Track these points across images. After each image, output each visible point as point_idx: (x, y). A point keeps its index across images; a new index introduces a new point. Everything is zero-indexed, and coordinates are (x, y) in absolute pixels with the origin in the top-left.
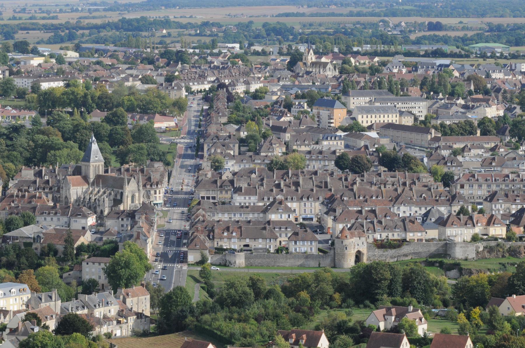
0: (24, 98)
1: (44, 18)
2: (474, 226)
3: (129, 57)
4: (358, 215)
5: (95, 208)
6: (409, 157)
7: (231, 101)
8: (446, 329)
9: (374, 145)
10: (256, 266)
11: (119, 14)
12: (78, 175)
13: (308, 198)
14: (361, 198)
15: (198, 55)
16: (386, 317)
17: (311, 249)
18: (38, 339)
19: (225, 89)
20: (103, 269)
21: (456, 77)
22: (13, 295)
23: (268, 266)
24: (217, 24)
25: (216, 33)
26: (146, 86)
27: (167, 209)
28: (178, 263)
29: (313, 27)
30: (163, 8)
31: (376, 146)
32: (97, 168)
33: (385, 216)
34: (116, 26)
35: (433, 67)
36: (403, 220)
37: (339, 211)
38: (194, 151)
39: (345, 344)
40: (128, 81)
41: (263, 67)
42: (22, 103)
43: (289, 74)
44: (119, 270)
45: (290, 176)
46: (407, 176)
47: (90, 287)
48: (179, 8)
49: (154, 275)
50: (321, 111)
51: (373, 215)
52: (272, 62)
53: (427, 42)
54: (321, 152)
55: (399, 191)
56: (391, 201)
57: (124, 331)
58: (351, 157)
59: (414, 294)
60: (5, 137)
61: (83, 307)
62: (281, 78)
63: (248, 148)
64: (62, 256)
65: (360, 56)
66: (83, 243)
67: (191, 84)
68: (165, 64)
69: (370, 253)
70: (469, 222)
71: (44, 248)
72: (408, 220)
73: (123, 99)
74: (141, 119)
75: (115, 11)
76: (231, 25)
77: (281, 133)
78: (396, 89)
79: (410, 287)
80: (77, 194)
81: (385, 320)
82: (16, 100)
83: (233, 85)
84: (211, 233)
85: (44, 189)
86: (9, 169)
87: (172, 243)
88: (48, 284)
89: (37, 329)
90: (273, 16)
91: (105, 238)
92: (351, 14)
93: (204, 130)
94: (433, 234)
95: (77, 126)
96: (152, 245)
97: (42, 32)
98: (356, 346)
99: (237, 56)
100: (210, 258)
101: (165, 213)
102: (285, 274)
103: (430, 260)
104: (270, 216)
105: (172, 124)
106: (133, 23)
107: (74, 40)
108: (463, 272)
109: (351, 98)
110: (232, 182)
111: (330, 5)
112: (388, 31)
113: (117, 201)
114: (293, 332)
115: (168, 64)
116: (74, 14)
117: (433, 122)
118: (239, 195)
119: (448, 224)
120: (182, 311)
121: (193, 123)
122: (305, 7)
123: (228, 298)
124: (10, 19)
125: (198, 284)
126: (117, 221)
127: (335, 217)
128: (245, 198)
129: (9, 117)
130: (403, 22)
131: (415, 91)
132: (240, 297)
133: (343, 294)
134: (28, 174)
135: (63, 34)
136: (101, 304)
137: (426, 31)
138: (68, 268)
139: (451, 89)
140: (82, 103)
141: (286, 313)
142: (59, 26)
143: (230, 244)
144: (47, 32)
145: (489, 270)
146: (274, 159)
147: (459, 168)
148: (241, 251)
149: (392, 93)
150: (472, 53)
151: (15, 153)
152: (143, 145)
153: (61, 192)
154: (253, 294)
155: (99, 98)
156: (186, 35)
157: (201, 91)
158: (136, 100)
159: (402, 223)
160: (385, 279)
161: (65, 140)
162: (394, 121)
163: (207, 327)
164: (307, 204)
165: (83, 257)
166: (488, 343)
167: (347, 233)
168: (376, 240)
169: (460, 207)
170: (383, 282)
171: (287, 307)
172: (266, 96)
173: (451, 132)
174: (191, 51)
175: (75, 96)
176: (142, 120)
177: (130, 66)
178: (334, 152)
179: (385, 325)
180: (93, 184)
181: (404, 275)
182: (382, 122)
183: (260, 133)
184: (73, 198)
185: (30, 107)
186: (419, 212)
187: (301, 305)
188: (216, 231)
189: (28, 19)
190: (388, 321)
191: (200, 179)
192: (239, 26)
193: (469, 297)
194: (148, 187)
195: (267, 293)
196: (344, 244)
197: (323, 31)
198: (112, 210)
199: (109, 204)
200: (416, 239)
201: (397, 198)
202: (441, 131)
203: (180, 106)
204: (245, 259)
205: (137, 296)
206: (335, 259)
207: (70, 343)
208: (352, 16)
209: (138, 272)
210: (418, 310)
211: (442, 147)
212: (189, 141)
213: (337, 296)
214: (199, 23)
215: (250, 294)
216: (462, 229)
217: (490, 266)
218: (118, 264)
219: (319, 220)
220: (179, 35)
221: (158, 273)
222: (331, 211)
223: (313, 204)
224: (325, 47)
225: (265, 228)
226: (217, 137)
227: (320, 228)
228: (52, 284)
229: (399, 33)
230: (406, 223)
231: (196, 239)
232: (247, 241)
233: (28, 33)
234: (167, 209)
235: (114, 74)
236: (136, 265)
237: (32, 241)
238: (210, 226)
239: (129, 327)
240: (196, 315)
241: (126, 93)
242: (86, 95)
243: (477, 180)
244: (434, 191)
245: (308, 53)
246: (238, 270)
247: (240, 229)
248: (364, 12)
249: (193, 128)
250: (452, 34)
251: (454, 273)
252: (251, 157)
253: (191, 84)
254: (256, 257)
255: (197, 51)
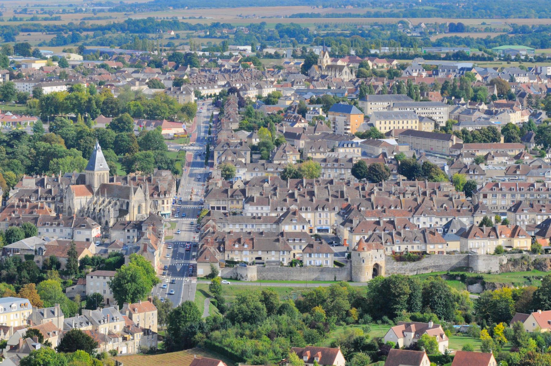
0: (25, 103)
1: (46, 19)
2: (498, 237)
3: (135, 60)
4: (375, 226)
5: (100, 219)
6: (429, 165)
7: (243, 107)
8: (468, 346)
9: (393, 153)
10: (269, 279)
11: (125, 14)
12: (81, 184)
13: (323, 209)
14: (379, 208)
15: (207, 57)
16: (405, 333)
17: (327, 262)
18: (40, 357)
19: (236, 94)
20: (108, 283)
21: (479, 81)
22: (14, 310)
23: (281, 280)
24: (227, 25)
25: (226, 35)
26: (154, 91)
27: (175, 220)
28: (187, 276)
29: (329, 29)
30: (171, 8)
31: (395, 154)
32: (101, 177)
33: (404, 228)
34: (121, 28)
35: (455, 71)
36: (423, 232)
37: (356, 222)
38: (203, 159)
39: (362, 362)
40: (134, 85)
41: (276, 70)
42: (23, 108)
43: (303, 77)
44: (125, 284)
45: (304, 185)
46: (427, 185)
47: (94, 302)
48: (188, 9)
49: (162, 289)
50: (337, 117)
51: (391, 226)
52: (286, 66)
53: (448, 44)
54: (337, 160)
55: (419, 200)
56: (411, 211)
57: (130, 348)
58: (368, 165)
59: (434, 309)
60: (5, 144)
61: (88, 323)
62: (295, 82)
63: (260, 156)
64: (65, 269)
65: (377, 59)
66: (87, 256)
67: (201, 88)
68: (173, 67)
69: (388, 266)
70: (493, 233)
71: (46, 260)
72: (428, 232)
73: (129, 105)
74: (148, 125)
75: (120, 11)
76: (243, 26)
77: (295, 140)
78: (416, 94)
79: (431, 302)
80: (81, 204)
81: (404, 336)
82: (16, 105)
83: (244, 89)
84: (221, 245)
85: (46, 199)
86: (9, 178)
87: (181, 256)
88: (50, 298)
89: (38, 346)
90: (286, 17)
91: (110, 251)
92: (368, 15)
93: (214, 137)
94: (454, 246)
95: (81, 132)
96: (160, 258)
97: (44, 33)
98: (373, 364)
99: (248, 59)
100: (220, 272)
101: (173, 224)
102: (299, 289)
103: (451, 273)
104: (283, 227)
105: (181, 130)
106: (140, 24)
107: (78, 42)
108: (486, 286)
109: (369, 103)
110: (243, 191)
111: (346, 5)
112: (408, 33)
113: (123, 212)
114: (307, 349)
115: (176, 68)
116: (78, 14)
117: (455, 129)
118: (251, 205)
119: (470, 236)
120: (191, 327)
121: (203, 129)
122: (321, 7)
123: (240, 313)
124: (10, 20)
125: (208, 299)
126: (123, 232)
127: (351, 228)
128: (257, 209)
129: (9, 123)
130: (423, 23)
131: (435, 96)
132: (252, 312)
133: (360, 309)
134: (30, 183)
135: (66, 36)
136: (106, 320)
137: (448, 33)
138: (72, 282)
139: (473, 93)
140: (85, 108)
141: (300, 329)
142: (62, 28)
143: (241, 256)
144: (49, 34)
145: (513, 283)
146: (288, 167)
147: (482, 177)
148: (253, 263)
149: (412, 97)
150: (495, 56)
151: (15, 161)
152: (150, 152)
153: (64, 202)
154: (265, 309)
155: (104, 103)
156: (195, 37)
157: (211, 96)
158: (142, 105)
159: (422, 235)
160: (404, 294)
161: (69, 147)
162: (414, 128)
163: (217, 344)
164: (322, 214)
165: (87, 271)
166: (512, 361)
167: (364, 245)
168: (394, 253)
169: (482, 218)
170: (402, 296)
171: (302, 323)
172: (279, 101)
173: (474, 139)
174: (201, 53)
175: (79, 101)
176: (149, 126)
177: (136, 69)
178: (351, 160)
179: (404, 342)
180: (98, 193)
181: (424, 289)
182: (401, 128)
183: (273, 140)
184: (77, 208)
185: (32, 113)
186: (440, 223)
187: (315, 321)
188: (227, 243)
189: (29, 20)
190: (407, 338)
191: (210, 188)
192: (251, 27)
193: (492, 313)
194: (156, 196)
195: (280, 308)
196: (361, 256)
197: (339, 32)
198: (117, 221)
199: (114, 214)
200: (437, 251)
201: (417, 208)
202: (463, 137)
203: (189, 112)
204: (257, 272)
205: (144, 311)
206: (351, 273)
207: (74, 361)
208: (369, 17)
209: (145, 286)
210: (438, 326)
211: (464, 154)
212: (198, 148)
213: (354, 311)
214: (209, 25)
215: (263, 309)
216: (485, 241)
217: (514, 280)
218: (124, 278)
219: (335, 232)
220: (188, 37)
221: (166, 287)
222: (347, 221)
223: (329, 214)
224: (342, 50)
225: (278, 240)
226: (228, 144)
227: (336, 240)
228: (55, 299)
229: (419, 35)
230: (426, 235)
231: (205, 252)
232: (260, 254)
233: (29, 35)
234: (175, 220)
235: (120, 78)
236: (143, 279)
237: (34, 254)
238: (220, 238)
239: (136, 344)
240: (206, 331)
241: (133, 98)
242: (90, 100)
243: (501, 189)
244: (455, 201)
245: (324, 56)
246: (250, 284)
247: (251, 241)
248: (382, 13)
249: (202, 134)
250: (475, 36)
251: (476, 287)
252: (263, 165)
253: (201, 88)
254: (269, 270)
255: (207, 54)
